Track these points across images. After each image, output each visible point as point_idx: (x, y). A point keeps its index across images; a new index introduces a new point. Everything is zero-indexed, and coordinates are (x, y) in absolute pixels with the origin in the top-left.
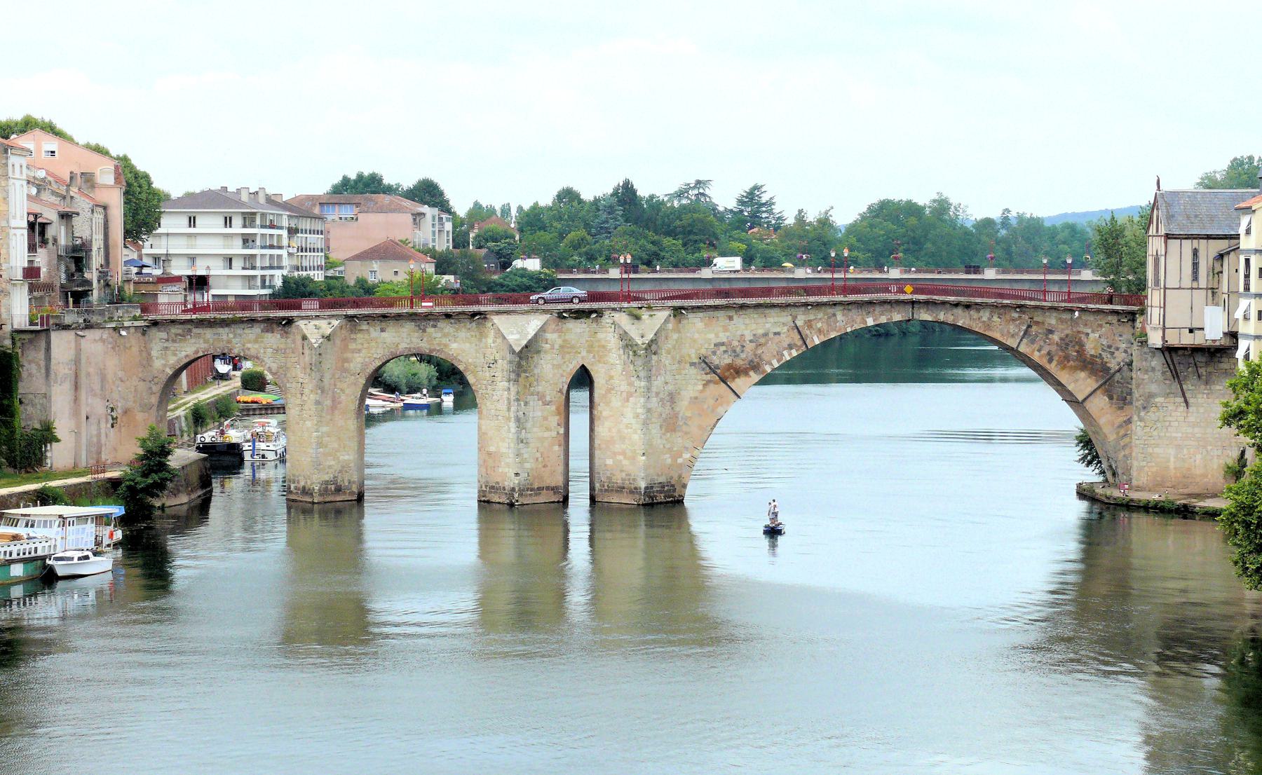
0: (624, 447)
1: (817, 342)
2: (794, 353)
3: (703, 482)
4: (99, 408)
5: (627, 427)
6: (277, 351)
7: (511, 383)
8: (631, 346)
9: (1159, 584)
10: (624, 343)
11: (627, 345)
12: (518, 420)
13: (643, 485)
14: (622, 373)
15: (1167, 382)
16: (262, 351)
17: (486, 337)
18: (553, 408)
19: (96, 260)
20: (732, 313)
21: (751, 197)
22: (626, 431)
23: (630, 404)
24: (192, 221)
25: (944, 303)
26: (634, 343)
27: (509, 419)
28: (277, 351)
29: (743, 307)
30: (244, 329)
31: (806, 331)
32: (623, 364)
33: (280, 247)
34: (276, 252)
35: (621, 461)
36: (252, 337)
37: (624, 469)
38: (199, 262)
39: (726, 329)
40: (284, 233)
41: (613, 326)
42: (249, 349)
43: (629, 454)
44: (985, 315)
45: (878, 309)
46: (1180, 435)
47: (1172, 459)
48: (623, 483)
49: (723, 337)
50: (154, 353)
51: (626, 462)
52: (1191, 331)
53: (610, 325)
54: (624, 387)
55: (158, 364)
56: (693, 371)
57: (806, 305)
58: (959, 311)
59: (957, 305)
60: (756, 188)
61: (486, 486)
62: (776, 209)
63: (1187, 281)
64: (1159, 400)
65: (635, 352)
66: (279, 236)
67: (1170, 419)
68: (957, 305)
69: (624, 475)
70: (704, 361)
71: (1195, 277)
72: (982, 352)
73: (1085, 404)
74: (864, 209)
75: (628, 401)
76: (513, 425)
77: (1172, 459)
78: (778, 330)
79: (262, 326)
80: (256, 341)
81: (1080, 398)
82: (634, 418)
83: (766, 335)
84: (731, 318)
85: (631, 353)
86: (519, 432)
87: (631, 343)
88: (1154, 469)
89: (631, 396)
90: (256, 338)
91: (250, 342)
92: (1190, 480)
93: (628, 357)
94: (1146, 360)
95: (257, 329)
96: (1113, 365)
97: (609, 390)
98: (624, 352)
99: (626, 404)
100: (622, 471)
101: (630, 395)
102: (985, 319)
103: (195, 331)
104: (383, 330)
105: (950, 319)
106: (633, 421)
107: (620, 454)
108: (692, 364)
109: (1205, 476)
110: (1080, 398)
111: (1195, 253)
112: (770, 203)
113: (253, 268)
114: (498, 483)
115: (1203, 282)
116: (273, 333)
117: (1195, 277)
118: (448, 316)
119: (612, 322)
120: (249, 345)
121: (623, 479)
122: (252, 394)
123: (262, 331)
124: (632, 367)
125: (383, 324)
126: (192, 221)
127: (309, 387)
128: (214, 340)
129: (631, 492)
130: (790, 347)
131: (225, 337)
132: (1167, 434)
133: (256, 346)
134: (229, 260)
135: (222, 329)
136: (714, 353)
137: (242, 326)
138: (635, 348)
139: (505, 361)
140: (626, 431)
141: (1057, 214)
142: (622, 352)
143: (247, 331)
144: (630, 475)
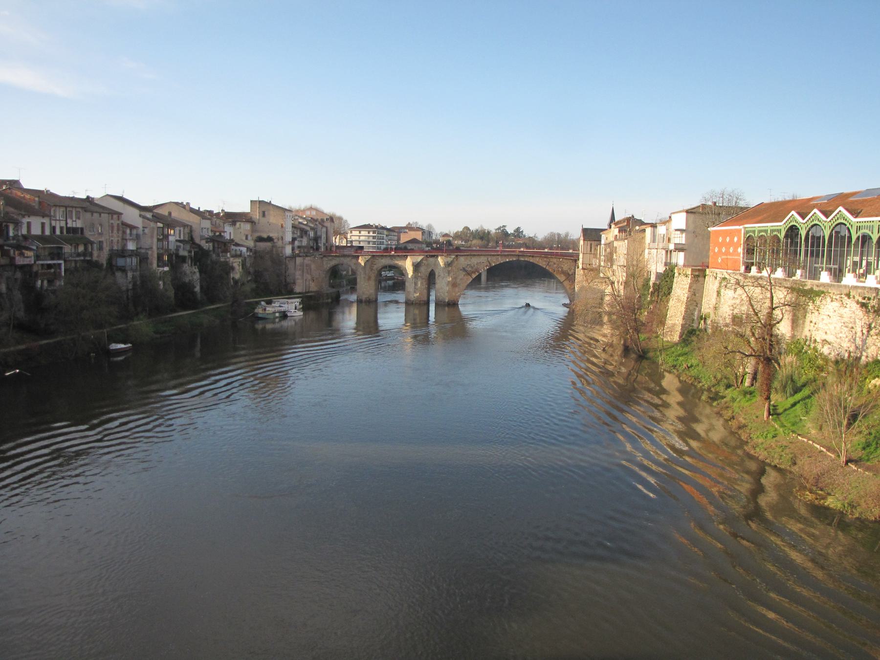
1: (493, 265)
2: (488, 268)
3: (856, 230)
4: (309, 277)
9: (851, 199)
12: (415, 283)
13: (447, 300)
18: (425, 280)
19: (323, 240)
20: (472, 257)
21: (518, 230)
24: (360, 233)
25: (527, 256)
27: (412, 283)
29: (474, 255)
31: (491, 262)
33: (383, 239)
34: (382, 240)
38: (361, 243)
39: (470, 261)
40: (385, 236)
44: (537, 259)
45: (510, 257)
49: (469, 263)
50: (324, 264)
51: (442, 295)
52: (589, 265)
55: (325, 267)
56: (461, 272)
57: (491, 255)
58: (531, 258)
59: (530, 256)
60: (519, 228)
62: (524, 233)
63: (589, 252)
66: (383, 237)
68: (530, 256)
70: (464, 269)
71: (591, 251)
72: (844, 240)
73: (563, 283)
76: (414, 284)
78: (483, 261)
81: (562, 281)
83: (480, 263)
84: (471, 258)
86: (415, 286)
95: (350, 258)
96: (570, 273)
97: (439, 276)
102: (538, 260)
103: (335, 258)
104: (382, 259)
105: (528, 260)
108: (461, 270)
110: (562, 281)
111: (591, 244)
112: (522, 232)
113: (375, 244)
115: (593, 252)
117: (591, 251)
118: (398, 256)
122: (644, 255)
126: (360, 233)
127: (362, 273)
130: (487, 266)
134: (369, 242)
136: (467, 267)
141: (64, 196)
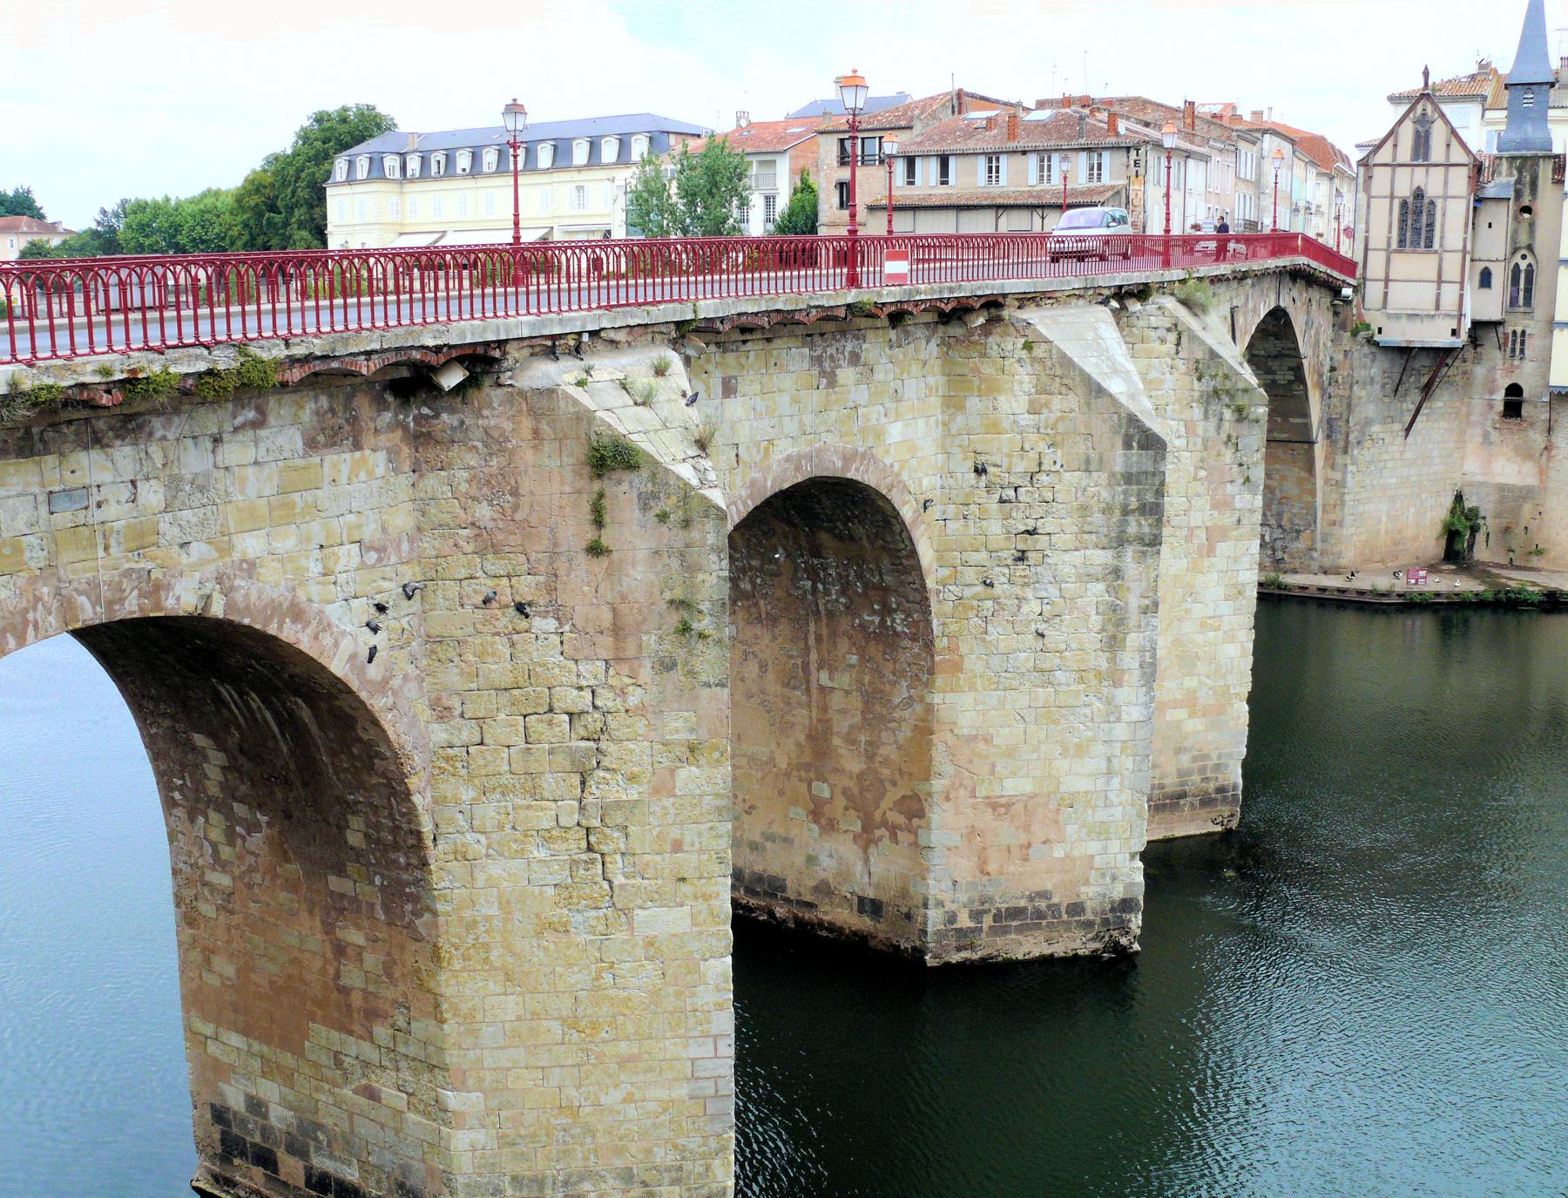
0: (1191, 683)
5: (1204, 626)
6: (381, 550)
7: (1130, 552)
8: (1227, 392)
10: (1208, 385)
11: (1216, 392)
14: (1196, 474)
15: (1386, 400)
16: (315, 568)
17: (990, 389)
22: (1199, 638)
23: (1219, 562)
26: (1241, 386)
28: (381, 550)
30: (217, 440)
32: (1199, 445)
35: (1178, 724)
36: (257, 485)
37: (1186, 744)
41: (1172, 337)
42: (250, 567)
43: (1206, 699)
46: (1394, 480)
47: (1384, 519)
48: (1183, 784)
51: (1194, 725)
53: (1161, 333)
54: (1202, 515)
61: (977, 915)
64: (1375, 428)
65: (1239, 410)
67: (1385, 457)
69: (1185, 761)
74: (258, 164)
75: (1211, 551)
77: (1384, 519)
79: (307, 413)
80: (282, 513)
82: (1227, 598)
85: (1228, 414)
87: (1228, 385)
88: (1363, 537)
89: (1224, 537)
90: (282, 491)
91: (252, 522)
92: (1401, 547)
93: (1219, 428)
94: (1365, 367)
98: (1206, 412)
99: (1206, 562)
100: (1179, 751)
101: (1215, 535)
106: (1225, 608)
107: (1176, 705)
109: (1415, 539)
114: (1044, 895)
116: (357, 446)
119: (1167, 323)
120: (250, 545)
121: (1180, 773)
123: (311, 444)
124: (1228, 455)
125: (731, 358)
128: (54, 541)
129: (1206, 801)
131: (116, 512)
132: (1381, 482)
133: (287, 542)
135: (96, 455)
137: (210, 420)
138: (1241, 400)
139: (1102, 477)
140: (1199, 638)
142: (1197, 412)
143: (236, 452)
144: (1206, 757)
